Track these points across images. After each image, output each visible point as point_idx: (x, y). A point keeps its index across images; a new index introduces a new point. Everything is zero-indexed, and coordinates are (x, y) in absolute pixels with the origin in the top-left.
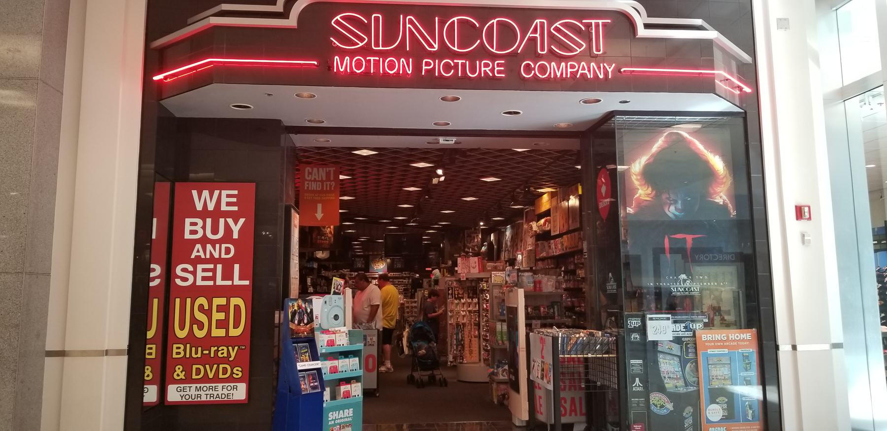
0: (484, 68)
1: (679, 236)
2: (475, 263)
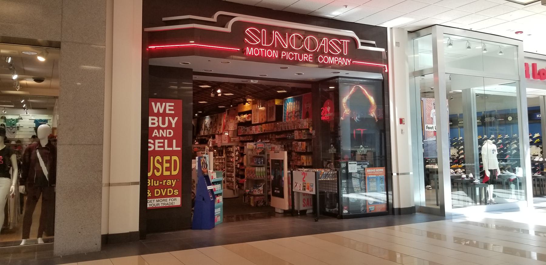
0: (305, 57)
1: (358, 130)
2: (226, 138)
